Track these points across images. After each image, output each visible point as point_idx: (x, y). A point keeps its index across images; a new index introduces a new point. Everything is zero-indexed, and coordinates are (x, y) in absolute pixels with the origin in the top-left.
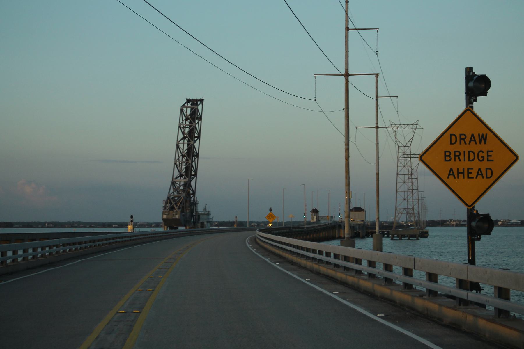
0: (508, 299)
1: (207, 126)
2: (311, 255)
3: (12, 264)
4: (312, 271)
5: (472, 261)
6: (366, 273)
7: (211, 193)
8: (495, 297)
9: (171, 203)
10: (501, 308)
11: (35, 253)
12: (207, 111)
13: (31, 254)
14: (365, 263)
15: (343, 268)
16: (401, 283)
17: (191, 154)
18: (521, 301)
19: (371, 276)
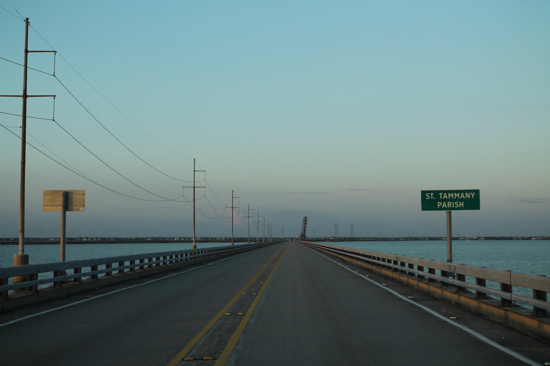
0: (434, 273)
1: (308, 222)
2: (381, 262)
3: (106, 278)
4: (394, 280)
5: (450, 261)
6: (416, 275)
7: (309, 235)
8: (501, 290)
9: (301, 236)
10: (539, 307)
11: (121, 267)
12: (308, 219)
13: (162, 261)
14: (426, 270)
15: (456, 289)
16: (475, 292)
17: (305, 227)
18: (549, 302)
19: (432, 280)
